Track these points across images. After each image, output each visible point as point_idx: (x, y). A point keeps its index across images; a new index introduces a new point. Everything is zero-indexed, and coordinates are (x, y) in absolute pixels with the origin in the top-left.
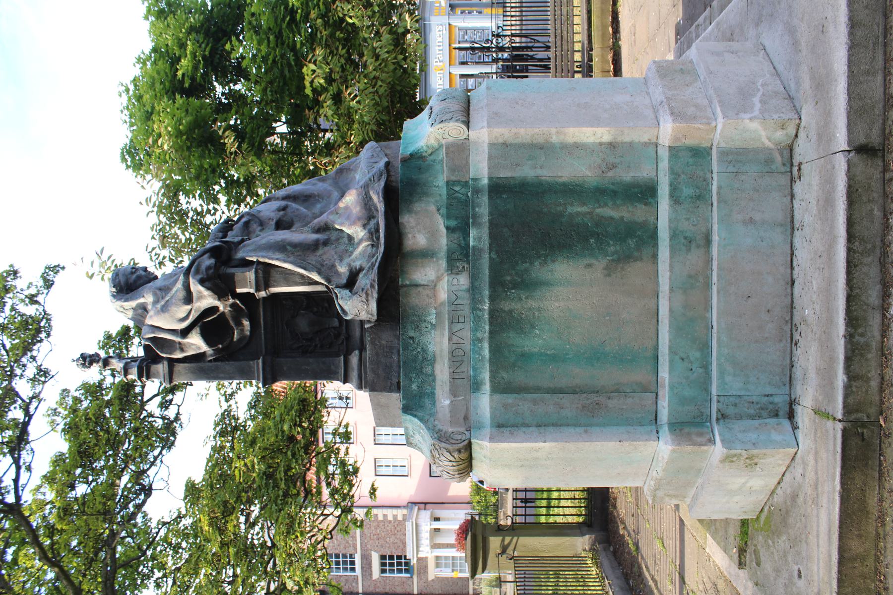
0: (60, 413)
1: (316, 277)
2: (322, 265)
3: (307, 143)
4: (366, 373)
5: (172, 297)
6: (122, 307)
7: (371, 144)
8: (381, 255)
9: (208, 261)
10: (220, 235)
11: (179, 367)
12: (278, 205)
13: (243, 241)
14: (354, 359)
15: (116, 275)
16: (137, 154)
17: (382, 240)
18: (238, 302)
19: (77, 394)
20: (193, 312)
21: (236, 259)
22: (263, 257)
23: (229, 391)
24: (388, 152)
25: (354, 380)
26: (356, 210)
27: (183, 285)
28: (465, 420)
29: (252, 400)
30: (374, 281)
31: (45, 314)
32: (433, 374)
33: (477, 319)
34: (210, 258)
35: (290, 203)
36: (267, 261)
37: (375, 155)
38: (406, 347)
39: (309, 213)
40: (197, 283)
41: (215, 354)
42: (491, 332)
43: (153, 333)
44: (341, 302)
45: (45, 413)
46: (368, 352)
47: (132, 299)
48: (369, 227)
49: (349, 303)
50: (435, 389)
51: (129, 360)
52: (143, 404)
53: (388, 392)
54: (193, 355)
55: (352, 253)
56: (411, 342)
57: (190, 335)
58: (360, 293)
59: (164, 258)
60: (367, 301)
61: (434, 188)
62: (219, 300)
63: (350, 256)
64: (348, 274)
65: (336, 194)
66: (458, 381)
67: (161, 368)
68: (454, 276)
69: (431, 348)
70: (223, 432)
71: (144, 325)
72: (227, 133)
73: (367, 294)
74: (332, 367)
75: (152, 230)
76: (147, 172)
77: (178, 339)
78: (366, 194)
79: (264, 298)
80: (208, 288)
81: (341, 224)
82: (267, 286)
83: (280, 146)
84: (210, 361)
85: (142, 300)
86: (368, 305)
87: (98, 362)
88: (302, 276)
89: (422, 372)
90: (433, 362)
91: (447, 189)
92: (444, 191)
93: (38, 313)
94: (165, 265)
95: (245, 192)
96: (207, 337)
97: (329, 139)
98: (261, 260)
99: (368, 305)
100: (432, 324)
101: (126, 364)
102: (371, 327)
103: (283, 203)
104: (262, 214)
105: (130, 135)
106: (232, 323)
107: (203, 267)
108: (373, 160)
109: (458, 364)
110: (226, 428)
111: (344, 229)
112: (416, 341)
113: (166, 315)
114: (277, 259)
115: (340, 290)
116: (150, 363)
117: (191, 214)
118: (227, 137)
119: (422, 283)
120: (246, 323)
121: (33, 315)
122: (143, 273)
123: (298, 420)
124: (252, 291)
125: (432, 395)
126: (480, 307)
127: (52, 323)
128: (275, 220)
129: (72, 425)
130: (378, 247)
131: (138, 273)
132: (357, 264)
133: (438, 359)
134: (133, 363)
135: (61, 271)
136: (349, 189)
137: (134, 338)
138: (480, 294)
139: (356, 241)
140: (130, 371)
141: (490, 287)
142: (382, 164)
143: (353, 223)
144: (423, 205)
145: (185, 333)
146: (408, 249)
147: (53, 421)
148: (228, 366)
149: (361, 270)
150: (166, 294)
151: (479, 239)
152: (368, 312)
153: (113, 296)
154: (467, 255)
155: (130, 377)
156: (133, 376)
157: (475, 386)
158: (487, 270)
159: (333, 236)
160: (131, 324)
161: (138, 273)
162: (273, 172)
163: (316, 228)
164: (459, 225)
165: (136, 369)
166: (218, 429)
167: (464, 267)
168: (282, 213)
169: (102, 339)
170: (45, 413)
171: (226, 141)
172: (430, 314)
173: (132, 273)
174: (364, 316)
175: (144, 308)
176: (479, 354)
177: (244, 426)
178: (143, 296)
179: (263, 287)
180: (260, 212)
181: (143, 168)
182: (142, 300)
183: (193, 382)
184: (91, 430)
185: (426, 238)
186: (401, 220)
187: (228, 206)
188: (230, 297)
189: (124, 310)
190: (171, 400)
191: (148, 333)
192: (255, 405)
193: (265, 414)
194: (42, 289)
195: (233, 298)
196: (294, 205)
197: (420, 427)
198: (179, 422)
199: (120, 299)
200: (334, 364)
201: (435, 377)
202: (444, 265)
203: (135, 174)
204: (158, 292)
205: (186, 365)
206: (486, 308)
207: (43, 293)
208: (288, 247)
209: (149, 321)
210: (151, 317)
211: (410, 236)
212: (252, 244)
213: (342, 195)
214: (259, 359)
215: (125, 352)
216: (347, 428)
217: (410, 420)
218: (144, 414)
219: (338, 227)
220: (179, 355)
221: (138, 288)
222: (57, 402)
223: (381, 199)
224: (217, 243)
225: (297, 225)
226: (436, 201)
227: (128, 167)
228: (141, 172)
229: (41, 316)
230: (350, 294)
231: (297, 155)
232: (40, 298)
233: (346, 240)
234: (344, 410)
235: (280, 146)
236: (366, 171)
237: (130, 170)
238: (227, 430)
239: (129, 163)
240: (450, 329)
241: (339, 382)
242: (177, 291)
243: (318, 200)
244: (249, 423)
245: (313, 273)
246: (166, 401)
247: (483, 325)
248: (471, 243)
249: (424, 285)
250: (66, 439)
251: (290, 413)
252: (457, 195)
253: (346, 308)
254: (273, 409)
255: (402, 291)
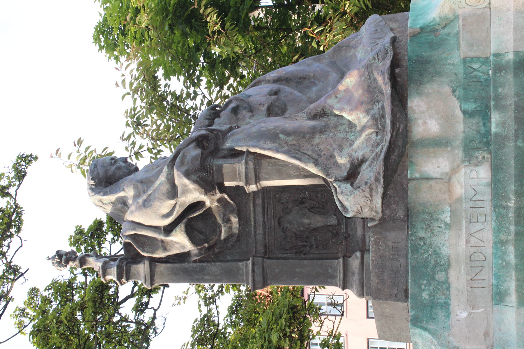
0: (28, 314)
1: (312, 169)
2: (320, 156)
3: (295, 17)
4: (369, 279)
5: (154, 191)
6: (100, 201)
7: (373, 19)
8: (387, 144)
9: (194, 152)
10: (207, 122)
11: (161, 268)
12: (269, 89)
13: (231, 129)
14: (355, 262)
15: (95, 166)
16: (111, 33)
17: (389, 128)
18: (226, 196)
19: (46, 294)
20: (177, 207)
21: (224, 150)
22: (253, 146)
23: (210, 294)
24: (394, 25)
25: (354, 286)
26: (358, 94)
27: (167, 178)
28: (485, 337)
29: (233, 304)
30: (379, 173)
31: (17, 206)
32: (447, 282)
33: (500, 218)
34: (195, 148)
35: (282, 86)
36: (258, 151)
37: (379, 30)
38: (416, 249)
39: (304, 97)
40: (182, 175)
41: (200, 254)
42: (517, 234)
43: (134, 229)
44: (341, 197)
45: (12, 313)
46: (372, 254)
47: (112, 192)
48: (373, 112)
49: (350, 198)
50: (449, 299)
51: (107, 259)
52: (117, 305)
53: (394, 300)
54: (176, 255)
55: (353, 142)
56: (422, 243)
57: (173, 233)
58: (363, 186)
59: (141, 147)
60: (371, 196)
61: (448, 67)
62: (206, 194)
63: (351, 145)
64: (348, 166)
65: (334, 76)
66: (477, 291)
67: (142, 268)
68: (472, 168)
69: (445, 251)
70: (202, 339)
71: (124, 221)
72: (209, 10)
73: (371, 189)
74: (330, 270)
75: (127, 118)
76: (122, 53)
77: (160, 237)
78: (369, 75)
79: (254, 192)
80: (195, 182)
81: (341, 110)
82: (257, 180)
83: (264, 20)
84: (195, 261)
85: (122, 194)
86: (371, 201)
87: (74, 260)
88: (297, 168)
89: (433, 278)
90: (446, 267)
91: (464, 67)
92: (461, 70)
93: (9, 206)
94: (142, 156)
95: (227, 73)
96: (190, 233)
97: (320, 11)
98: (252, 150)
99: (371, 201)
100: (446, 224)
101: (105, 263)
102: (375, 226)
103: (275, 87)
104: (251, 99)
105: (103, 13)
106: (219, 220)
107: (189, 158)
108: (377, 36)
109: (478, 270)
110: (205, 335)
111: (344, 115)
112: (428, 243)
113: (149, 210)
114: (269, 149)
115: (339, 183)
116: (129, 262)
117: (169, 98)
118: (208, 15)
119: (434, 176)
120: (234, 220)
121: (4, 207)
122: (123, 164)
123: (288, 330)
124: (242, 184)
125: (446, 306)
126: (504, 204)
127: (23, 217)
128: (266, 105)
129: (41, 328)
130: (383, 136)
131: (118, 164)
132: (359, 155)
133: (453, 263)
134: (112, 263)
135: (33, 161)
136: (349, 69)
137: (107, 233)
138: (504, 188)
139: (358, 128)
140: (109, 271)
141: (516, 181)
142: (387, 40)
143: (355, 108)
144: (435, 86)
145: (168, 230)
146: (418, 137)
147: (21, 323)
148: (215, 268)
149: (363, 161)
150: (148, 188)
151: (503, 124)
152: (371, 209)
153: (91, 189)
154: (487, 144)
155: (109, 277)
156: (112, 276)
157: (498, 297)
158: (513, 161)
159: (332, 121)
160: (104, 219)
161: (118, 164)
162: (258, 50)
163: (312, 114)
164: (478, 109)
165: (115, 269)
166: (196, 336)
167: (484, 157)
168: (274, 97)
169: (74, 235)
170: (12, 313)
171: (208, 20)
172: (443, 212)
173: (112, 164)
174: (366, 213)
175: (123, 203)
176: (503, 260)
177: (224, 334)
178: (124, 190)
179: (254, 180)
180: (249, 96)
181: (119, 48)
182: (122, 194)
183: (170, 284)
184: (62, 334)
185: (439, 124)
186: (409, 105)
187: (208, 88)
188: (217, 191)
189: (102, 205)
190: (147, 304)
191: (129, 230)
192: (237, 310)
193: (248, 321)
194: (14, 180)
195: (221, 192)
196: (286, 89)
197: (432, 343)
198: (154, 327)
199: (98, 193)
200: (331, 267)
201: (449, 285)
202: (460, 156)
203: (108, 55)
204: (139, 185)
205: (168, 265)
206: (511, 205)
207: (15, 185)
208: (281, 136)
209: (129, 217)
210: (132, 212)
211: (420, 122)
212: (241, 132)
213: (342, 76)
214: (248, 260)
215: (97, 248)
216: (338, 339)
217: (420, 335)
218: (116, 318)
219: (337, 113)
220: (160, 255)
221: (118, 180)
222: (25, 302)
223: (387, 80)
224: (203, 132)
225: (290, 111)
226: (451, 81)
227: (101, 48)
228: (116, 53)
229: (12, 210)
230: (351, 188)
231: (284, 30)
232: (12, 191)
233: (346, 127)
234: (338, 318)
235: (264, 20)
236: (369, 49)
237: (104, 51)
238: (206, 337)
239: (102, 44)
240: (468, 229)
241: (338, 288)
242: (160, 184)
243: (314, 83)
244: (229, 330)
245: (310, 165)
246: (142, 304)
247: (507, 225)
248: (493, 130)
249: (436, 178)
250: (34, 343)
251: (279, 322)
252: (475, 73)
253: (346, 204)
254: (257, 315)
255: (411, 185)
